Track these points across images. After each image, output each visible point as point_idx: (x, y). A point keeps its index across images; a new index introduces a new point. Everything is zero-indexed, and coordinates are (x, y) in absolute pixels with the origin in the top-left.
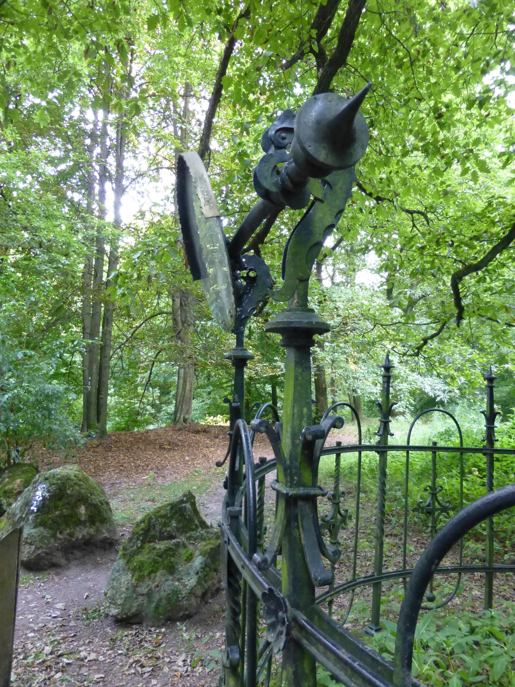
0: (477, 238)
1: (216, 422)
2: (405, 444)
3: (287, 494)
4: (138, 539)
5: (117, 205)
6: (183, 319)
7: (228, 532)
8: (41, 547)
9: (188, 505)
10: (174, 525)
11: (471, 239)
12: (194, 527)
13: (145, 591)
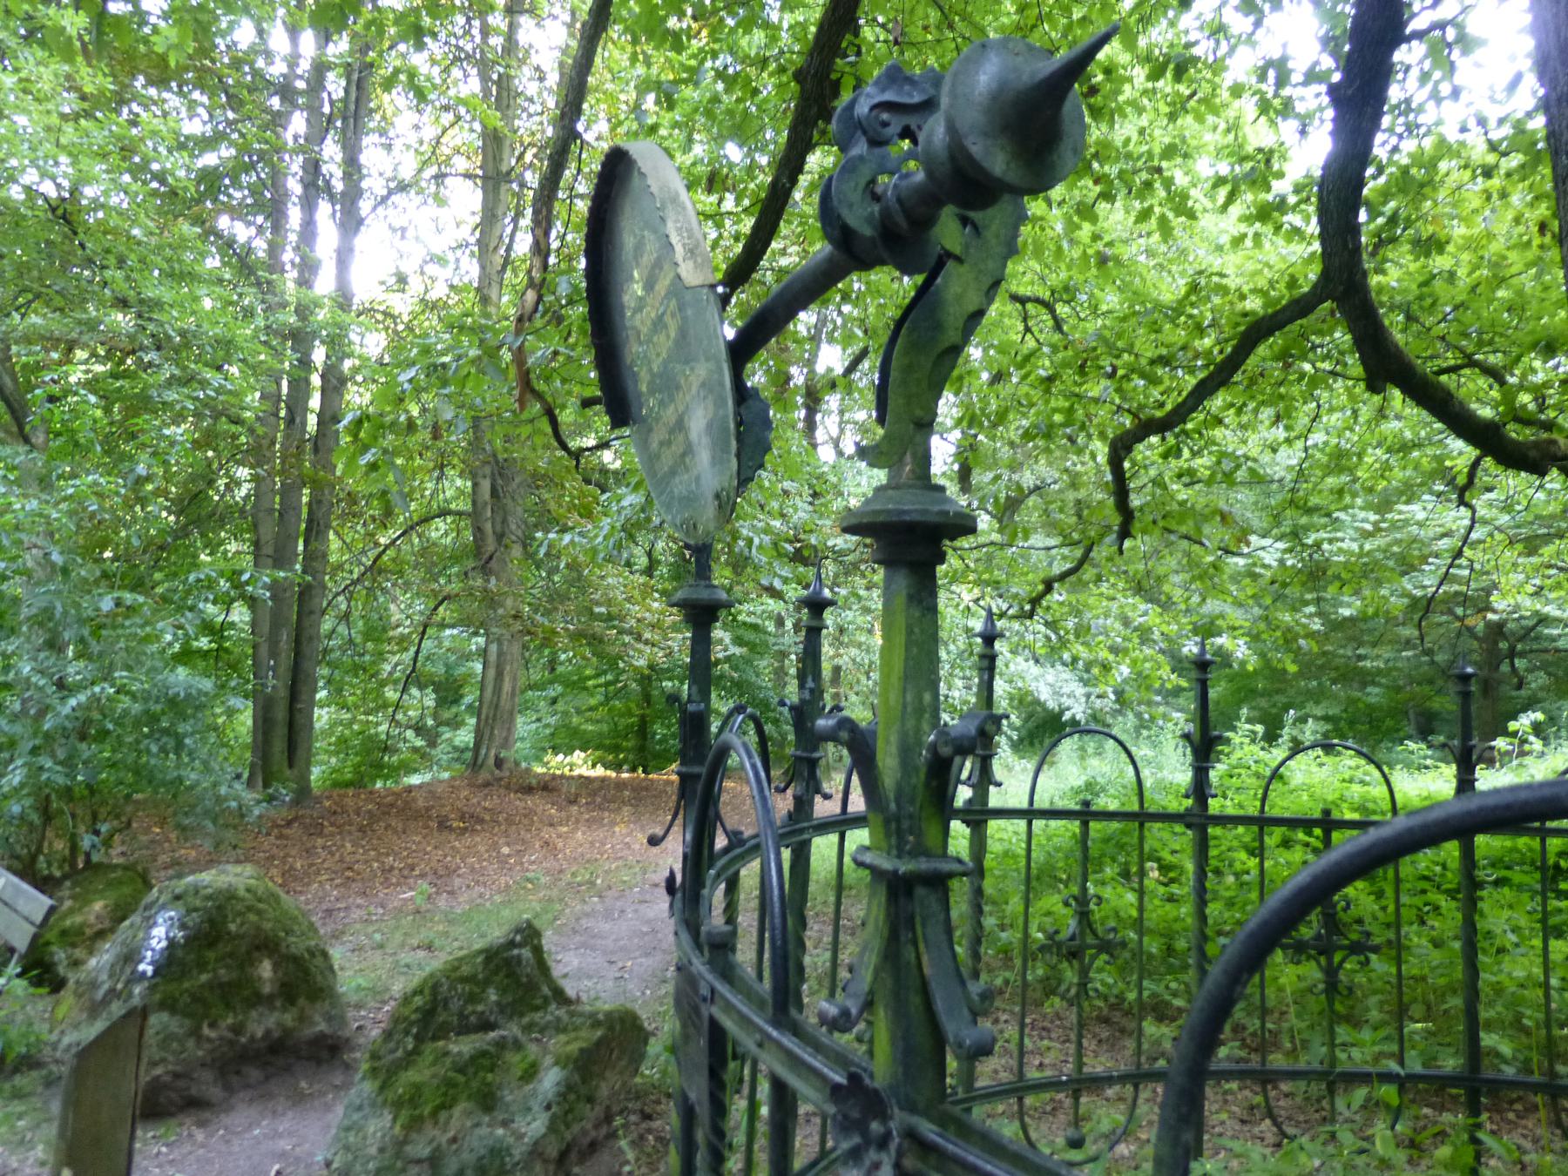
0: (1163, 361)
1: (572, 766)
2: (1025, 805)
3: (895, 872)
4: (407, 1033)
5: (344, 257)
6: (498, 528)
7: (710, 977)
8: (163, 1060)
9: (526, 953)
10: (494, 998)
11: (1152, 362)
12: (539, 1002)
13: (425, 1152)
